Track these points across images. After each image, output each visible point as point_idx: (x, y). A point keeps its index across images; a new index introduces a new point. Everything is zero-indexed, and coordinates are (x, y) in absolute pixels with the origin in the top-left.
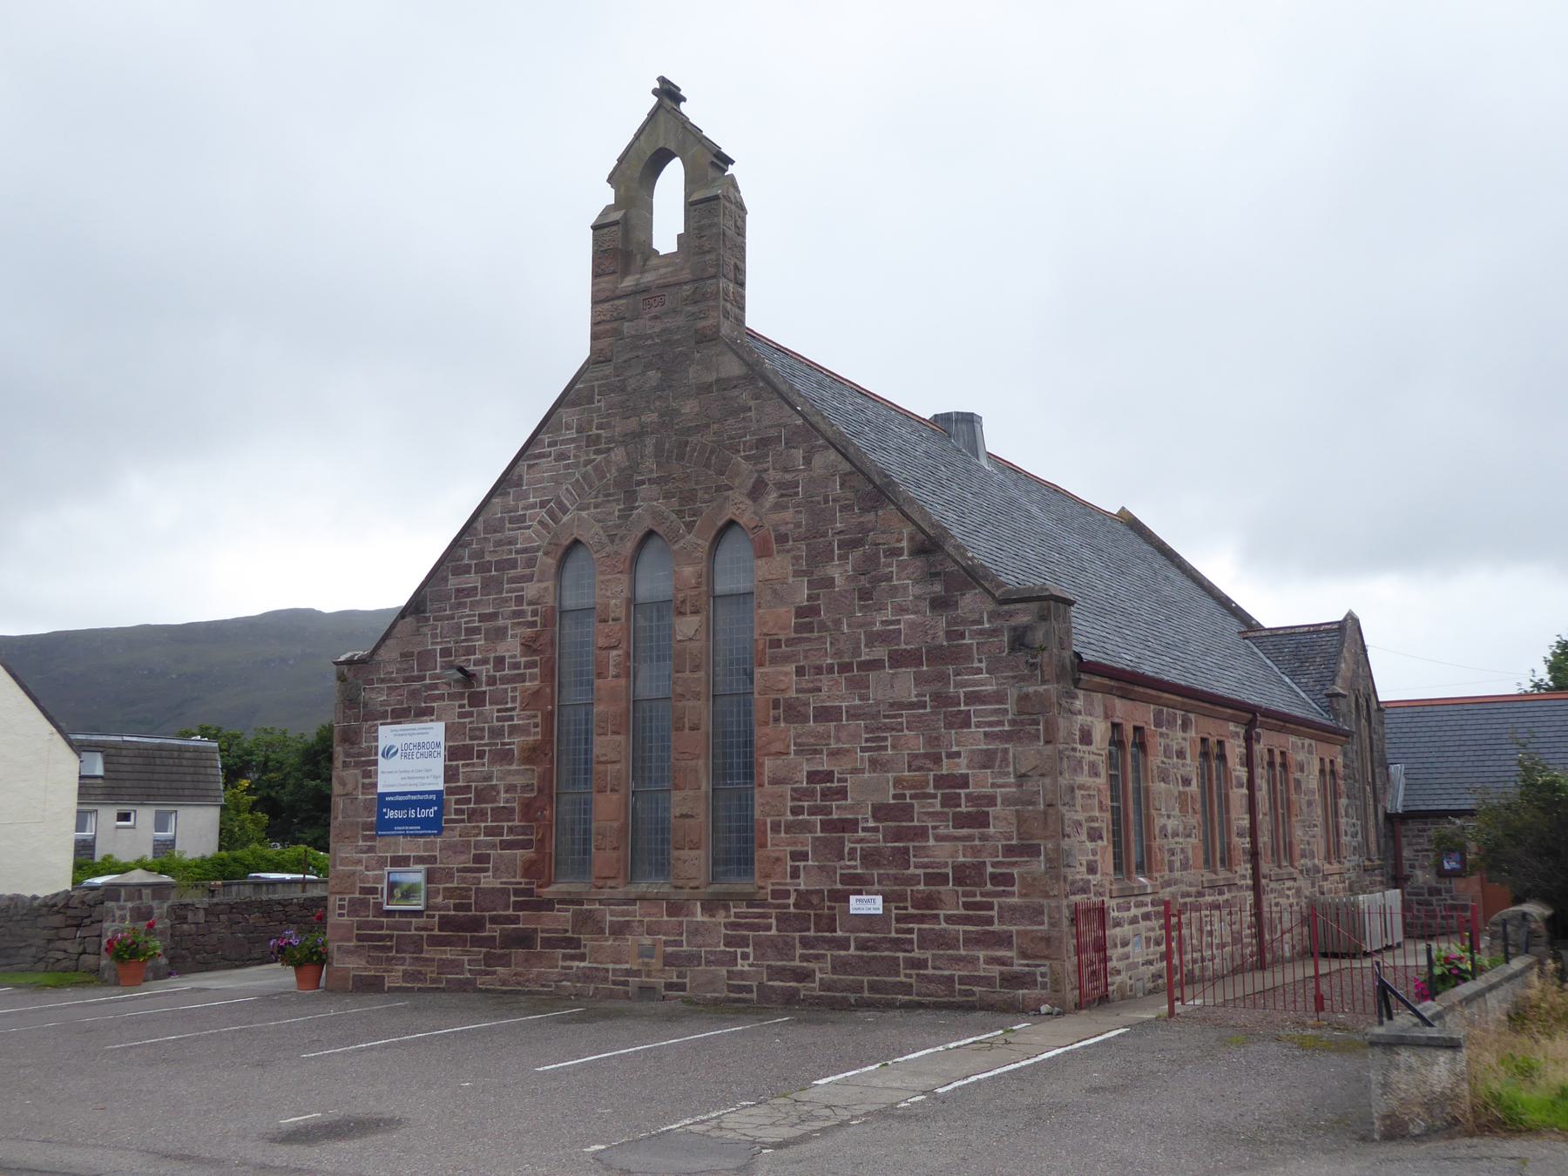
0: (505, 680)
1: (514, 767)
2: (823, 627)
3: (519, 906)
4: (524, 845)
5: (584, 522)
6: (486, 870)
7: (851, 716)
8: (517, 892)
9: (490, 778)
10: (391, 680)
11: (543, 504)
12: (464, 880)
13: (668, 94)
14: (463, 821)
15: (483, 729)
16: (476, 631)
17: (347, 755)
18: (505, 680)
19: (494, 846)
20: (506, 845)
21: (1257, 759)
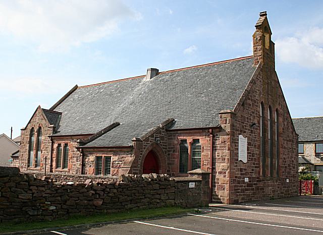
3: (257, 181)
10: (240, 122)
16: (251, 115)
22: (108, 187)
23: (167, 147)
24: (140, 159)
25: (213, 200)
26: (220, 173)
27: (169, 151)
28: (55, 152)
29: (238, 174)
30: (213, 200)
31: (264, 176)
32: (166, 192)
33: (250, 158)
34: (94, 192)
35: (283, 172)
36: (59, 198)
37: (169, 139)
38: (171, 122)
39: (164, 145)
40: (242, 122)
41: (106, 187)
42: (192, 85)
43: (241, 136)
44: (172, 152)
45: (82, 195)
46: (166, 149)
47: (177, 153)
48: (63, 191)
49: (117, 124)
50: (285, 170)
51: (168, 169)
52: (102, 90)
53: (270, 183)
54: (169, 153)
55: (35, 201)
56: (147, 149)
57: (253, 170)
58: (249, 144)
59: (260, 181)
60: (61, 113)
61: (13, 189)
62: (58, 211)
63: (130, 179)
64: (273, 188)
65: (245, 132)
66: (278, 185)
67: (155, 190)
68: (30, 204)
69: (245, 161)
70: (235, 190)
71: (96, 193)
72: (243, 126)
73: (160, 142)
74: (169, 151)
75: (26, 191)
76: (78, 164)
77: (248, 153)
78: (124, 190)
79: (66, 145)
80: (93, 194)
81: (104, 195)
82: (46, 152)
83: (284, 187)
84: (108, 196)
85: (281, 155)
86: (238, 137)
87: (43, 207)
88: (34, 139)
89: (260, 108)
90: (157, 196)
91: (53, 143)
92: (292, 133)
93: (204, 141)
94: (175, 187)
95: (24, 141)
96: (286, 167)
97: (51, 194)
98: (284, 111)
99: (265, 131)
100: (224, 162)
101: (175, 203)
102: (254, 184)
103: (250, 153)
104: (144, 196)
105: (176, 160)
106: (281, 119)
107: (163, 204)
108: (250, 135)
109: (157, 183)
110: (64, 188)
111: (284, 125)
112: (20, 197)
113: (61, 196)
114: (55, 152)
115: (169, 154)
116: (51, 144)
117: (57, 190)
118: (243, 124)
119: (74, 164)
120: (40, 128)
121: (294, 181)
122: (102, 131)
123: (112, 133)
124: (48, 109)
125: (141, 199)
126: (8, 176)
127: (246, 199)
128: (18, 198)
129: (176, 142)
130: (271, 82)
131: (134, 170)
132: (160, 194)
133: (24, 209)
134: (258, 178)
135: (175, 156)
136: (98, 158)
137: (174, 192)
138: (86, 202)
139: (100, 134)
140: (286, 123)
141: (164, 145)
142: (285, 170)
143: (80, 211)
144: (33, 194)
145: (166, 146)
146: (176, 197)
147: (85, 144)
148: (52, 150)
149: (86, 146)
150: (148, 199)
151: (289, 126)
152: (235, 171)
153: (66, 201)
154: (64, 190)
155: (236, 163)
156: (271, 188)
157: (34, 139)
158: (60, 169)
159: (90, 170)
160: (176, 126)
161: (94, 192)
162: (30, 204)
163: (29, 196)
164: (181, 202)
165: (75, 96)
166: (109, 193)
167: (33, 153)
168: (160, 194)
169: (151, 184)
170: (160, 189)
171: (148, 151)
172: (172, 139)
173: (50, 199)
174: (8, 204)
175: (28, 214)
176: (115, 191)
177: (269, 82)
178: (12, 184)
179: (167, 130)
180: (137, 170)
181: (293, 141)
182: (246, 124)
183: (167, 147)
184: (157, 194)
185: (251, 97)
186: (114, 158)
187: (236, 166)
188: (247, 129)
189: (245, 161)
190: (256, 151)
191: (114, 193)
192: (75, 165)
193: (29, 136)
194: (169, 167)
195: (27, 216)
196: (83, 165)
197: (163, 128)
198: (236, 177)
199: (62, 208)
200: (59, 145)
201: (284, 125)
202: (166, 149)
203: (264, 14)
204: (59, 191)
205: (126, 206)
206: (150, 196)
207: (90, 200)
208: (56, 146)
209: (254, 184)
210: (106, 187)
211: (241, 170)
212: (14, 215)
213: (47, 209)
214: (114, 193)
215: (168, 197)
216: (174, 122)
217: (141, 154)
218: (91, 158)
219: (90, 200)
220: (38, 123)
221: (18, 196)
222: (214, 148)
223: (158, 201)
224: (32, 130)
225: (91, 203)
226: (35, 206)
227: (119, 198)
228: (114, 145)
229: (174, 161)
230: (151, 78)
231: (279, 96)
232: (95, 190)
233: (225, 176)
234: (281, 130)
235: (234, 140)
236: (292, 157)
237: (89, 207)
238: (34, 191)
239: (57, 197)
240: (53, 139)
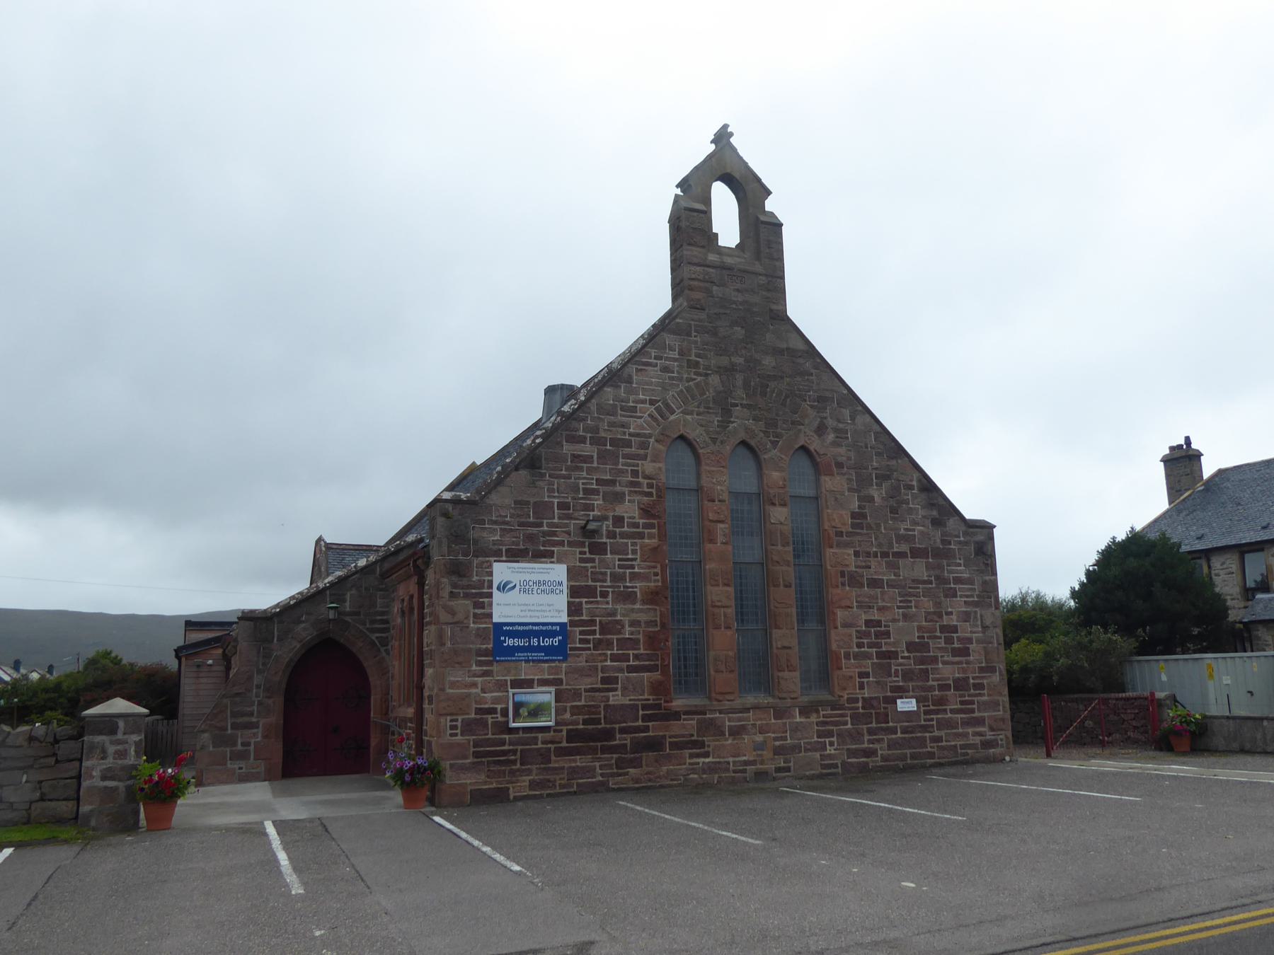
1: (637, 606)
3: (646, 718)
11: (652, 402)
152: (478, 691)
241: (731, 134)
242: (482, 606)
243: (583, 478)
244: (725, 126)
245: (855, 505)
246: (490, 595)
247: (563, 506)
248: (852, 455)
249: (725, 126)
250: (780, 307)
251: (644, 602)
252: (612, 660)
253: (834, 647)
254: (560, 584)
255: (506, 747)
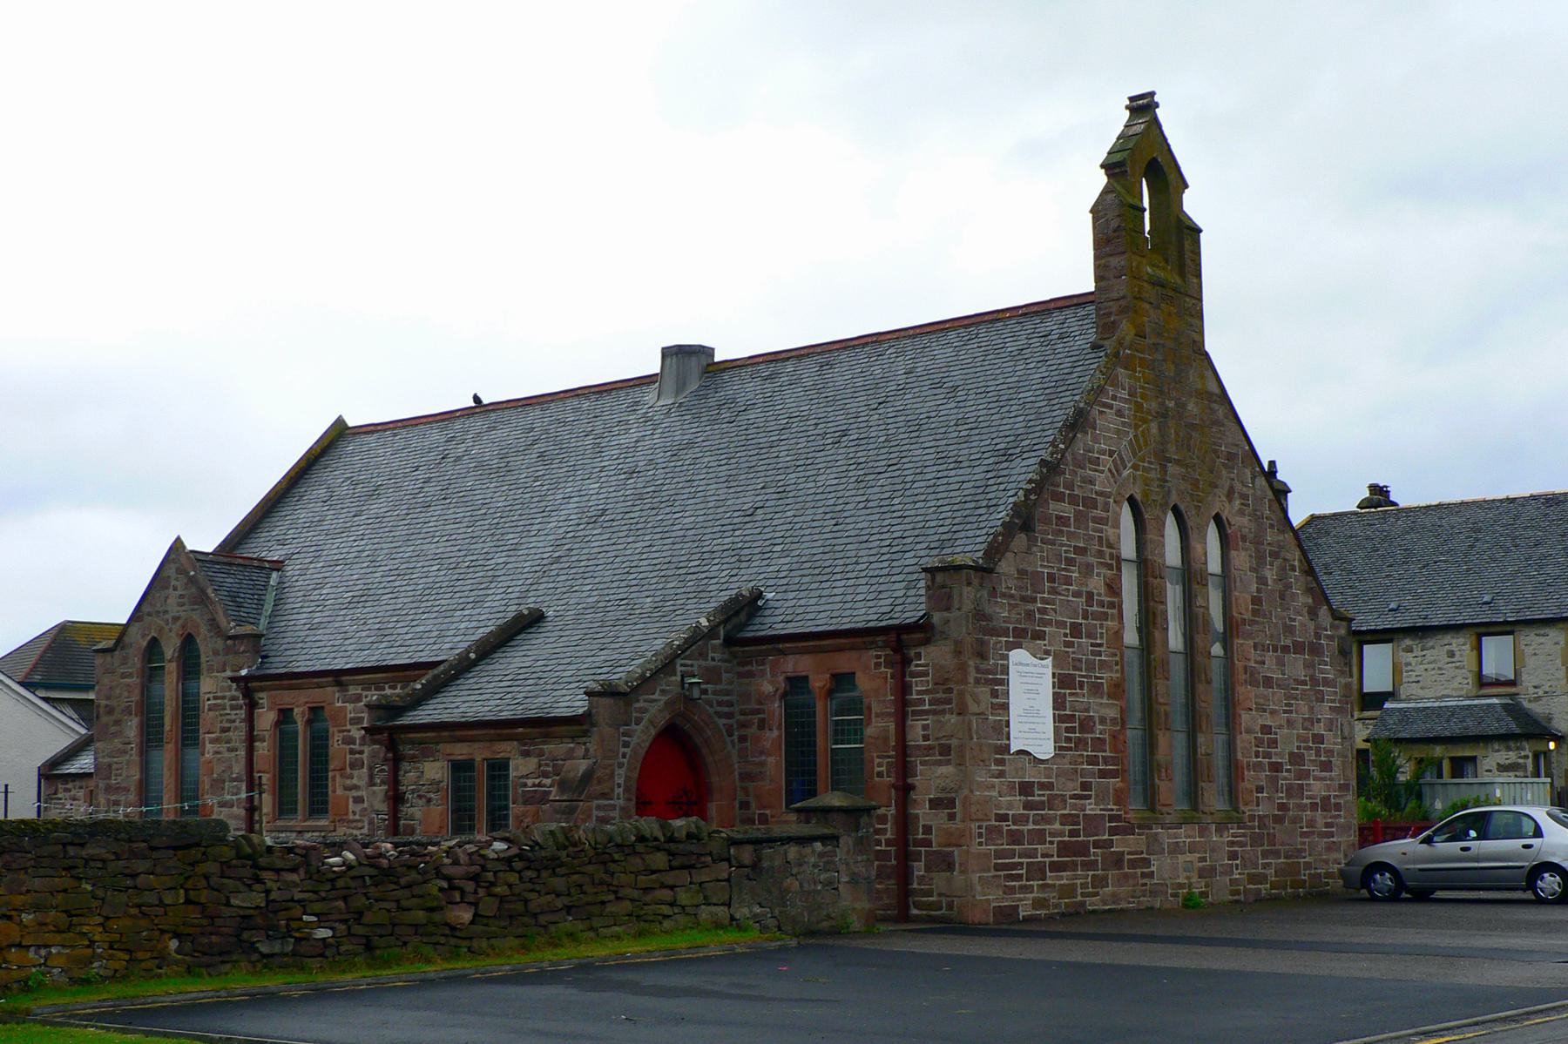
0: (1096, 616)
1: (1105, 701)
2: (1264, 616)
3: (1113, 831)
4: (1113, 774)
5: (660, 457)
6: (1089, 797)
7: (1279, 686)
8: (1112, 818)
9: (1087, 710)
10: (1012, 596)
11: (1111, 454)
12: (1074, 807)
13: (1143, 107)
14: (1070, 749)
15: (1080, 660)
16: (1070, 562)
17: (978, 670)
18: (1096, 616)
19: (1092, 775)
20: (1103, 774)
21: (1178, 721)
22: (489, 866)
23: (736, 709)
24: (621, 765)
25: (915, 912)
26: (935, 804)
27: (743, 725)
28: (263, 749)
29: (1010, 806)
30: (915, 912)
31: (1153, 810)
32: (697, 879)
33: (1068, 740)
34: (445, 884)
35: (1260, 789)
36: (341, 904)
37: (741, 675)
38: (747, 606)
39: (720, 704)
40: (1023, 599)
41: (484, 868)
42: (845, 433)
43: (1018, 656)
44: (753, 730)
45: (407, 893)
46: (729, 715)
47: (775, 733)
48: (352, 884)
49: (528, 623)
50: (1274, 781)
51: (740, 796)
52: (462, 448)
53: (1184, 835)
54: (743, 732)
55: (275, 912)
56: (651, 722)
57: (1085, 786)
58: (1063, 682)
59: (1128, 830)
60: (278, 566)
61: (214, 880)
62: (339, 944)
63: (561, 839)
64: (1203, 859)
65: (1040, 636)
66: (1232, 843)
67: (653, 872)
68: (259, 921)
69: (1044, 748)
70: (998, 867)
71: (452, 888)
72: (1030, 614)
73: (705, 692)
74: (743, 725)
75: (249, 886)
76: (376, 798)
77: (1058, 719)
78: (544, 874)
79: (315, 712)
80: (441, 889)
81: (476, 892)
82: (223, 747)
83: (1265, 855)
84: (489, 895)
85: (1245, 717)
86: (1006, 658)
87: (298, 930)
88: (169, 688)
89: (1117, 525)
90: (665, 894)
91: (252, 706)
92: (1313, 613)
93: (871, 677)
94: (728, 860)
95: (113, 703)
96: (1276, 768)
97: (315, 892)
98: (1256, 517)
99: (1150, 619)
100: (948, 763)
101: (732, 918)
102: (1096, 844)
103: (1071, 718)
104: (615, 892)
105: (771, 760)
106: (1241, 559)
107: (682, 919)
108: (1069, 644)
109: (658, 849)
110: (353, 873)
111: (1262, 581)
112: (234, 901)
113: (345, 898)
114: (263, 749)
115: (743, 739)
116: (242, 713)
117: (332, 880)
118: (1030, 607)
119: (358, 793)
120: (188, 642)
121: (1327, 825)
122: (468, 650)
123: (515, 660)
124: (209, 549)
125: (603, 903)
126: (198, 845)
127: (1056, 906)
128: (228, 904)
129: (768, 688)
130: (1181, 406)
131: (599, 808)
132: (672, 888)
133: (246, 935)
134: (1112, 818)
135: (768, 745)
136: (461, 768)
137: (728, 880)
138: (421, 913)
139: (463, 667)
140: (1270, 574)
141: (720, 704)
142: (1274, 781)
143: (405, 943)
144: (268, 892)
145: (730, 704)
146: (735, 897)
147: (399, 710)
148: (251, 739)
149: (406, 720)
150: (627, 904)
151: (1288, 586)
152: (995, 794)
153: (360, 913)
154: (353, 878)
155: (1001, 762)
156: (1189, 857)
157: (169, 688)
158: (297, 822)
159: (427, 815)
160: (775, 623)
161: (445, 884)
162: (259, 921)
163: (258, 899)
164: (756, 916)
165: (333, 476)
166: (493, 884)
167: (164, 759)
168: (672, 888)
169: (636, 853)
170: (672, 868)
171: (653, 732)
172: (751, 675)
173: (317, 907)
174: (205, 922)
175: (256, 950)
176: (513, 878)
177: (1171, 404)
178: (211, 867)
179: (729, 642)
180: (613, 807)
181: (1315, 650)
182: (1044, 601)
183: (736, 709)
184: (663, 886)
185: (1070, 486)
186: (520, 767)
187: (1001, 774)
188: (1049, 623)
189: (1044, 748)
190: (1103, 709)
191: (510, 886)
192: (359, 800)
193: (135, 680)
194: (746, 790)
195: (255, 957)
196: (396, 799)
197: (712, 632)
198: (1004, 818)
199: (350, 934)
200: (285, 715)
201: (1262, 581)
202: (729, 715)
203: (1143, 107)
204: (340, 883)
205: (552, 928)
206: (636, 894)
207: (431, 910)
208: (266, 718)
209: (1096, 844)
210: (484, 868)
211: (1026, 789)
212: (220, 954)
213: (307, 938)
214: (510, 886)
215: (705, 898)
216: (760, 603)
217: (626, 745)
218: (435, 770)
219: (431, 910)
220: (176, 619)
221: (228, 899)
222: (903, 708)
223: (666, 910)
224: (154, 646)
225: (436, 917)
226: (275, 928)
227: (526, 901)
228: (519, 713)
229: (763, 764)
230: (678, 392)
231: (1231, 457)
232: (449, 879)
233: (952, 817)
234: (1243, 608)
235: (989, 672)
236: (1312, 721)
237: (431, 929)
238: (269, 884)
239: (336, 899)
240: (248, 688)
241: (1157, 105)
242: (995, 694)
243: (1065, 546)
244: (178, 539)
245: (1254, 587)
246: (506, 808)
247: (1051, 578)
248: (1252, 526)
249: (178, 539)
250: (1196, 337)
251: (1109, 697)
252: (1106, 763)
253: (1240, 756)
254: (877, 715)
255: (1016, 860)
